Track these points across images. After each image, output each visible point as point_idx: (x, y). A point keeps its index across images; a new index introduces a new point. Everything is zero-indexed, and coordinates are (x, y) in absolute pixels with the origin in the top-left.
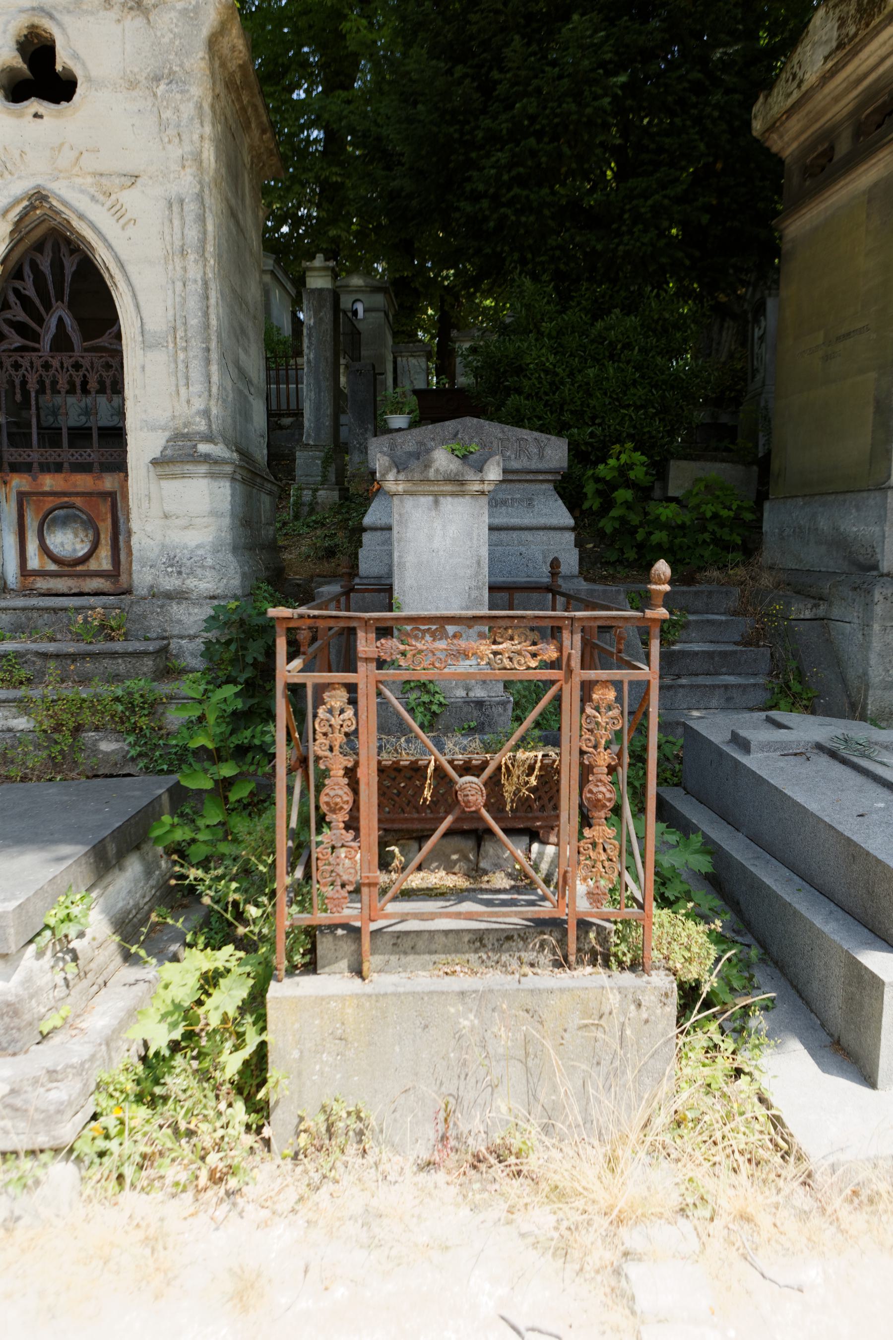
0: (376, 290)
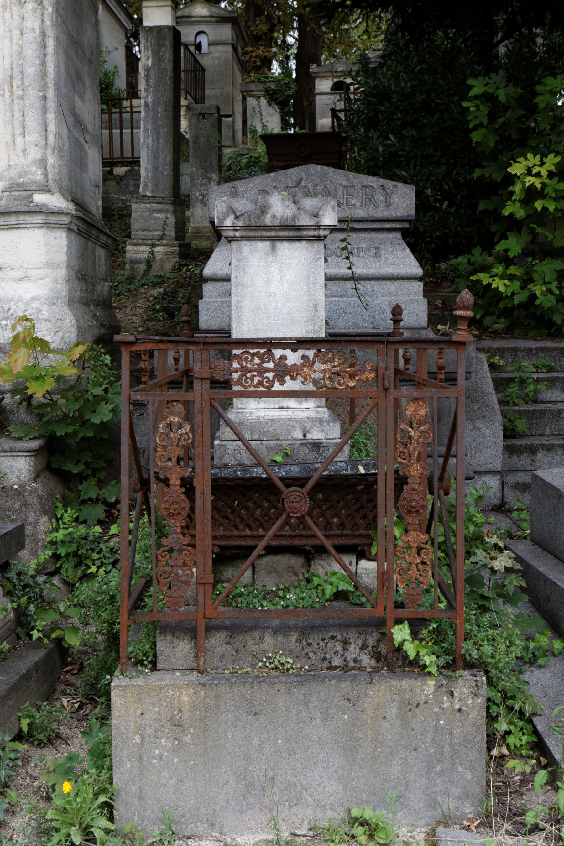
0: (221, 20)
